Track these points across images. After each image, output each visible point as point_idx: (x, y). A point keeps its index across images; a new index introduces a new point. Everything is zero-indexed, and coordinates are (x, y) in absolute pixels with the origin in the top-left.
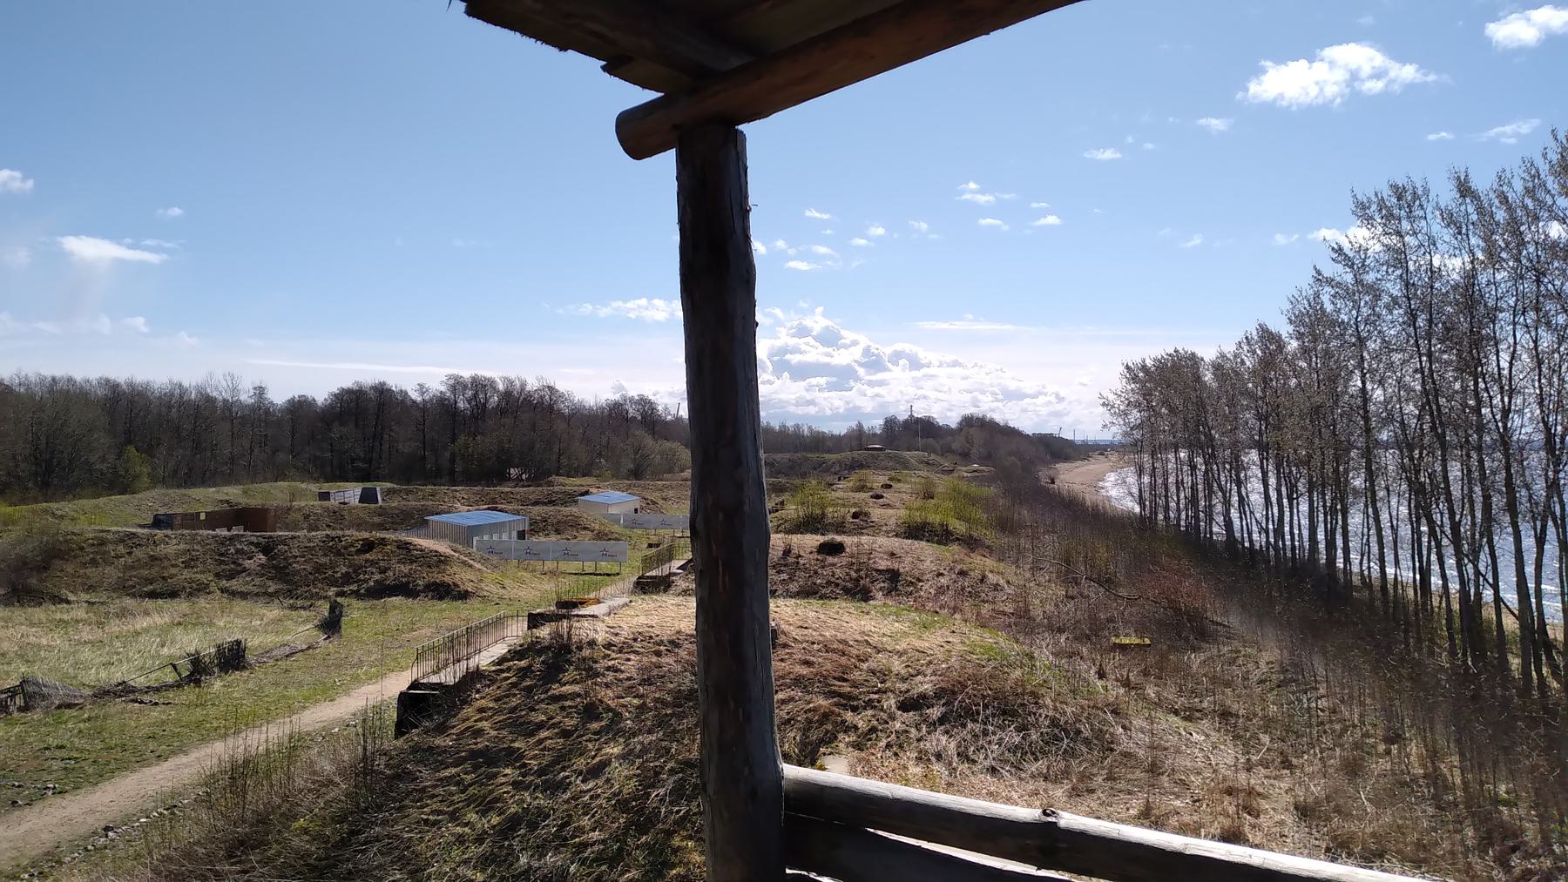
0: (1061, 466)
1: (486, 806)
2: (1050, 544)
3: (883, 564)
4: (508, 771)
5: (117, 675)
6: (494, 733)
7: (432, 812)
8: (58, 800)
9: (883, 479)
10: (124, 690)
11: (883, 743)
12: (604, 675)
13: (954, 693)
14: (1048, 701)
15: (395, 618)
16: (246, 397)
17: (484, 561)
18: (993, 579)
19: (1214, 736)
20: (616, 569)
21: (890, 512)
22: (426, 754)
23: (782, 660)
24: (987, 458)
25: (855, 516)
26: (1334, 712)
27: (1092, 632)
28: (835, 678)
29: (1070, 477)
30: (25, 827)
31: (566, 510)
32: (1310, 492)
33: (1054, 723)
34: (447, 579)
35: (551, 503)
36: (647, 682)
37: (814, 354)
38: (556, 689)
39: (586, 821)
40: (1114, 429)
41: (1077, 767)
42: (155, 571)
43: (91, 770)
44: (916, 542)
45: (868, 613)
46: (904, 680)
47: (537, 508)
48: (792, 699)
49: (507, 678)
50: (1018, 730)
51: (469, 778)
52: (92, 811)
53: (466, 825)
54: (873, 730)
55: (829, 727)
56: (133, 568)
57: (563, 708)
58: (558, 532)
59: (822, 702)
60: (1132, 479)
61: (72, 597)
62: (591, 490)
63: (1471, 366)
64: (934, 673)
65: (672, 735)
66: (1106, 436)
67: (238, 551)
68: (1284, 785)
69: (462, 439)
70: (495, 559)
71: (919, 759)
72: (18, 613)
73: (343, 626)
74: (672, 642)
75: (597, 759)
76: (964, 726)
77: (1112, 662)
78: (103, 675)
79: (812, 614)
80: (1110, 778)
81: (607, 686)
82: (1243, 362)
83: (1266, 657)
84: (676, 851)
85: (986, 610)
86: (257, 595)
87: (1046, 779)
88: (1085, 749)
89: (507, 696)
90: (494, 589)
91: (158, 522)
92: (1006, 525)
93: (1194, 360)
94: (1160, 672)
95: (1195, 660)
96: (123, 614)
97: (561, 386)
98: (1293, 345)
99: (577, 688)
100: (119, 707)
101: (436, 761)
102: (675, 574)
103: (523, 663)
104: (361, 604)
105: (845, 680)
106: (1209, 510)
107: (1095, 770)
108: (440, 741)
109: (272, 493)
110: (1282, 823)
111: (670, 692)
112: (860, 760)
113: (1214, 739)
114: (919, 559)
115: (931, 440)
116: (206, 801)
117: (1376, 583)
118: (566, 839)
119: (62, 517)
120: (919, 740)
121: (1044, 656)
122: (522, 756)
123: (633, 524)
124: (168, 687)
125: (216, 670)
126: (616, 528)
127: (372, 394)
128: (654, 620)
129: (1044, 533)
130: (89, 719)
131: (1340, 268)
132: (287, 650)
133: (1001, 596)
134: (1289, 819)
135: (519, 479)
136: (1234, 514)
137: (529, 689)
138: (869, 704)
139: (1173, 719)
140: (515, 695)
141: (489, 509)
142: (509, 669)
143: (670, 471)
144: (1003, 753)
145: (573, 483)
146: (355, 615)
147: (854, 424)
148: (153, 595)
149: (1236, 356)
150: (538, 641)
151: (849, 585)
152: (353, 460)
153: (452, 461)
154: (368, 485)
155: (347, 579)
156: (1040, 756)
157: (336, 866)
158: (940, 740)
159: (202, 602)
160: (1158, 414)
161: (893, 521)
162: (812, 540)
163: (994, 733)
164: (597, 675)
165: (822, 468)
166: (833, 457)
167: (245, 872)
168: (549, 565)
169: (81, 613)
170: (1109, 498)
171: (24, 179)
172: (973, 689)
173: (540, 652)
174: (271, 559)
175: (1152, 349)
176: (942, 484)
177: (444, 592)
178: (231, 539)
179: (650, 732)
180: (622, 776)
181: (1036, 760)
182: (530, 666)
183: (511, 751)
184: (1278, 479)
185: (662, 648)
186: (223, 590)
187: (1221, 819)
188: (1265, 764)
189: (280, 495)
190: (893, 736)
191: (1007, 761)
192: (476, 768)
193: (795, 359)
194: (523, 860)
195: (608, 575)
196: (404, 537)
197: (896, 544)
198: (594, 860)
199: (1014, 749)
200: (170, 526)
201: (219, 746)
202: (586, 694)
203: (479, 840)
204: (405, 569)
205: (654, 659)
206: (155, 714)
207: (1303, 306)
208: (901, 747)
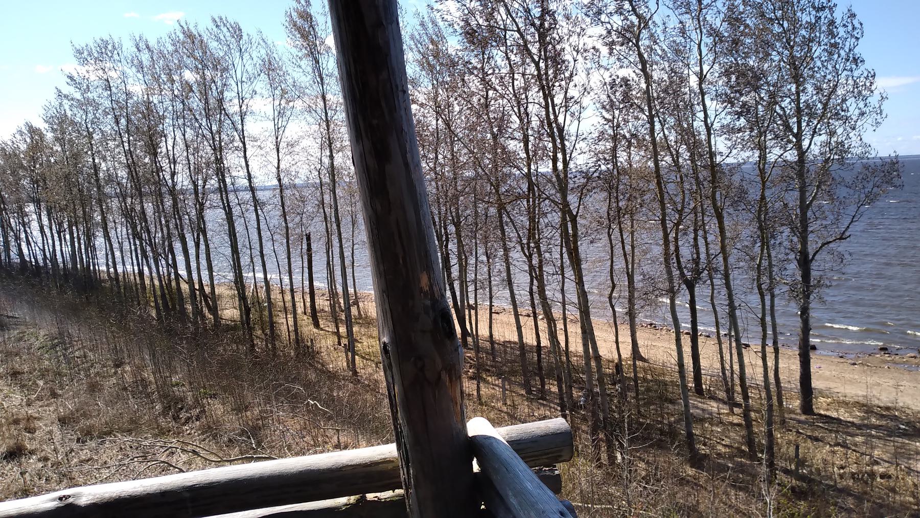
63: (153, 150)
83: (42, 333)
134: (55, 429)
136: (24, 246)
184: (50, 220)
188: (39, 399)
207: (53, 112)
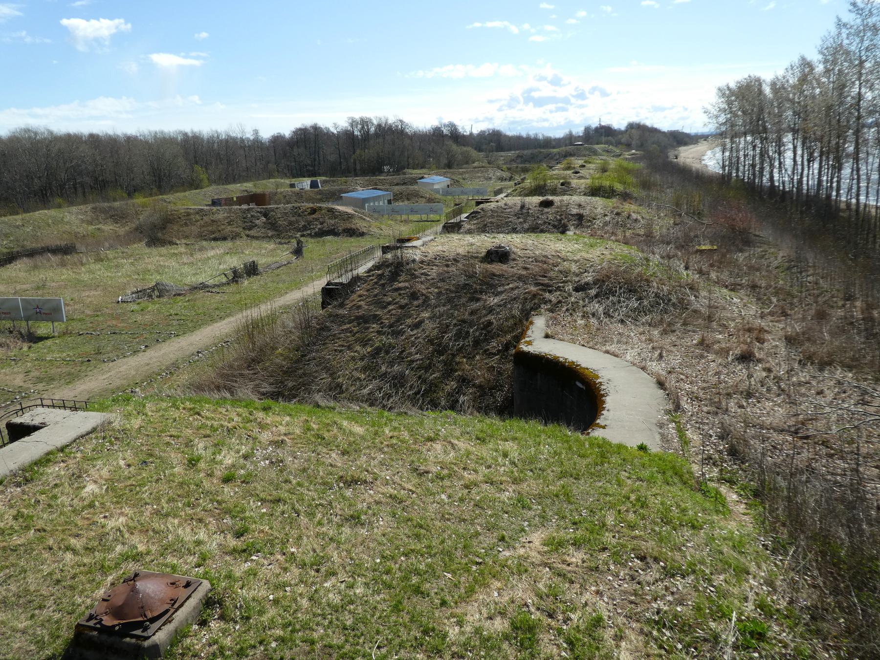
0: (682, 149)
1: (365, 343)
2: (669, 194)
3: (575, 211)
4: (374, 326)
5: (201, 279)
6: (366, 307)
7: (339, 346)
8: (176, 339)
9: (581, 162)
10: (203, 287)
11: (564, 309)
12: (420, 278)
13: (603, 281)
14: (655, 284)
15: (328, 247)
16: (250, 135)
17: (371, 216)
18: (634, 216)
19: (746, 299)
20: (438, 218)
21: (583, 181)
22: (334, 318)
23: (512, 267)
24: (641, 147)
25: (562, 184)
26: (816, 283)
27: (685, 244)
28: (540, 276)
29: (686, 155)
30: (163, 352)
31: (411, 187)
32: (821, 156)
33: (657, 295)
34: (353, 226)
35: (404, 184)
36: (443, 280)
37: (546, 91)
38: (397, 285)
39: (413, 350)
40: (710, 126)
41: (667, 318)
42: (214, 228)
43: (190, 325)
44: (593, 198)
45: (561, 240)
46: (577, 275)
47: (397, 187)
48: (517, 287)
49: (372, 280)
50: (637, 300)
51: (355, 329)
52: (192, 344)
53: (356, 352)
54: (560, 302)
55: (536, 301)
56: (204, 226)
57: (400, 294)
58: (408, 199)
59: (533, 289)
60: (719, 155)
61: (178, 242)
62: (425, 176)
64: (594, 271)
65: (455, 307)
66: (706, 130)
67: (252, 216)
68: (781, 326)
69: (358, 152)
70: (376, 215)
71: (583, 316)
72: (154, 251)
73: (304, 252)
74: (455, 260)
75: (418, 319)
76: (608, 298)
77: (694, 259)
78: (194, 279)
79: (531, 242)
80: (685, 324)
81: (422, 283)
82: (788, 81)
84: (458, 363)
85: (628, 233)
86: (263, 237)
87: (650, 325)
88: (672, 309)
89: (372, 289)
90: (376, 230)
91: (214, 203)
92: (646, 185)
93: (759, 82)
94: (719, 265)
95: (741, 257)
96: (201, 249)
97: (406, 120)
98: (820, 68)
99: (407, 284)
100: (202, 295)
101: (340, 321)
102: (463, 221)
103: (380, 272)
104: (313, 240)
105: (545, 277)
106: (762, 169)
107: (677, 320)
108: (341, 312)
109: (267, 185)
110: (776, 346)
111: (454, 285)
112: (551, 318)
113: (745, 301)
114: (594, 207)
115: (610, 138)
116: (238, 340)
117: (854, 207)
118: (403, 359)
119: (169, 202)
120: (584, 307)
121: (656, 259)
122: (380, 319)
123: (446, 193)
124: (223, 284)
125: (245, 275)
126: (438, 196)
127: (312, 131)
128: (445, 248)
129: (667, 188)
130: (188, 301)
131: (853, 16)
132: (277, 265)
133: (638, 225)
135: (389, 171)
137: (383, 285)
138: (558, 289)
139: (725, 290)
140: (376, 288)
141: (373, 189)
142: (373, 275)
143: (467, 163)
144: (628, 312)
145: (416, 172)
146: (310, 246)
147: (567, 131)
148: (215, 239)
149: (784, 77)
150: (386, 261)
151: (556, 223)
152: (306, 166)
153: (355, 163)
154: (314, 179)
155: (305, 228)
156: (648, 313)
157: (296, 371)
158: (597, 307)
159: (238, 242)
160: (736, 115)
161: (583, 186)
162: (536, 200)
163: (624, 302)
164: (416, 277)
165: (549, 157)
166: (555, 150)
167: (255, 374)
168: (404, 217)
169: (182, 249)
170: (706, 166)
171: (126, 23)
172: (614, 279)
173: (388, 266)
174: (268, 219)
175: (734, 78)
176: (613, 163)
177: (352, 233)
178: (248, 210)
179: (444, 306)
180: (430, 327)
181: (646, 315)
182: (383, 273)
183: (375, 316)
184: (803, 150)
185: (450, 263)
186: (248, 236)
187: (742, 345)
188: (772, 314)
189: (272, 186)
190: (570, 305)
191: (629, 317)
192: (359, 324)
193: (535, 95)
194: (383, 368)
195: (433, 221)
196: (330, 205)
197: (582, 199)
198: (418, 368)
199: (634, 310)
200: (220, 205)
201: (240, 316)
202: (412, 287)
203: (362, 359)
204: (332, 222)
205: (446, 269)
206: (218, 297)
208: (574, 310)
